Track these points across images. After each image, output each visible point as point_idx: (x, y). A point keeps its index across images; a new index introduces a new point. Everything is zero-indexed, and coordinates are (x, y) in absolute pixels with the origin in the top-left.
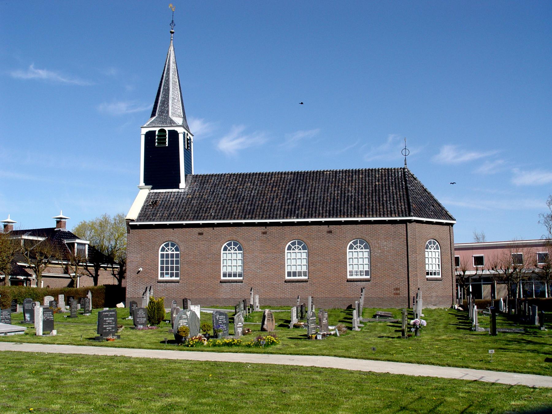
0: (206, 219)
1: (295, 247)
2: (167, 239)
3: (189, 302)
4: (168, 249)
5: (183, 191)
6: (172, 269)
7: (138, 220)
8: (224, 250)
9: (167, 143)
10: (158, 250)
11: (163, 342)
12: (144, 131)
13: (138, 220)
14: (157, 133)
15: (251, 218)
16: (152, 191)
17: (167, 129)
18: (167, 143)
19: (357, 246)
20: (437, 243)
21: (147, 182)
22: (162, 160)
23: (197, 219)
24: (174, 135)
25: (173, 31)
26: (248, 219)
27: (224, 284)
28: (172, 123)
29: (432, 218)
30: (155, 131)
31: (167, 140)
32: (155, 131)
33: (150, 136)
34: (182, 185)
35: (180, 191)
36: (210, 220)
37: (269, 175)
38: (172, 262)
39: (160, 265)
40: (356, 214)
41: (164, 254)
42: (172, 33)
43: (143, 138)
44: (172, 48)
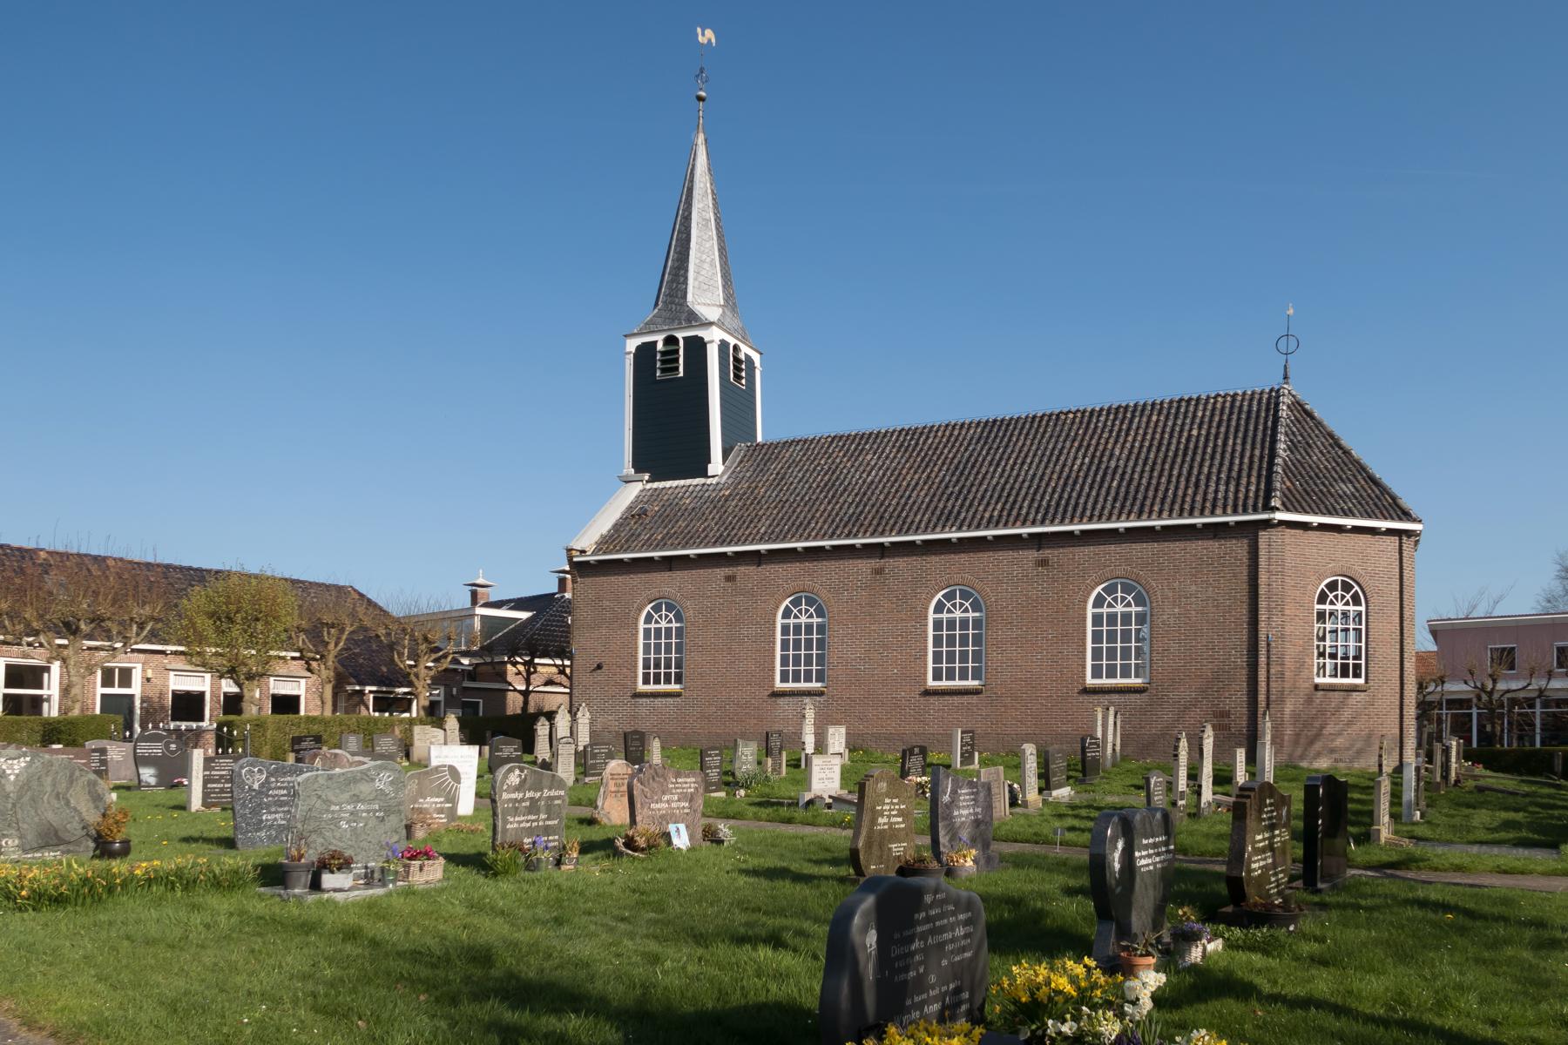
0: (744, 544)
1: (954, 605)
2: (654, 592)
3: (740, 742)
4: (1115, 599)
5: (714, 481)
6: (808, 662)
7: (593, 554)
8: (784, 617)
9: (681, 369)
10: (927, 609)
11: (187, 840)
12: (632, 345)
13: (593, 554)
14: (660, 346)
15: (847, 536)
16: (649, 486)
17: (680, 335)
18: (681, 369)
19: (1336, 597)
20: (1356, 588)
21: (639, 466)
22: (669, 410)
23: (722, 545)
24: (697, 347)
25: (703, 94)
26: (839, 537)
27: (781, 701)
28: (692, 319)
29: (1307, 512)
30: (655, 343)
31: (681, 360)
32: (655, 343)
33: (645, 351)
34: (716, 466)
35: (709, 481)
36: (751, 543)
37: (1134, 412)
38: (964, 640)
39: (931, 649)
40: (1116, 511)
41: (1101, 615)
42: (700, 99)
43: (629, 362)
44: (701, 138)
